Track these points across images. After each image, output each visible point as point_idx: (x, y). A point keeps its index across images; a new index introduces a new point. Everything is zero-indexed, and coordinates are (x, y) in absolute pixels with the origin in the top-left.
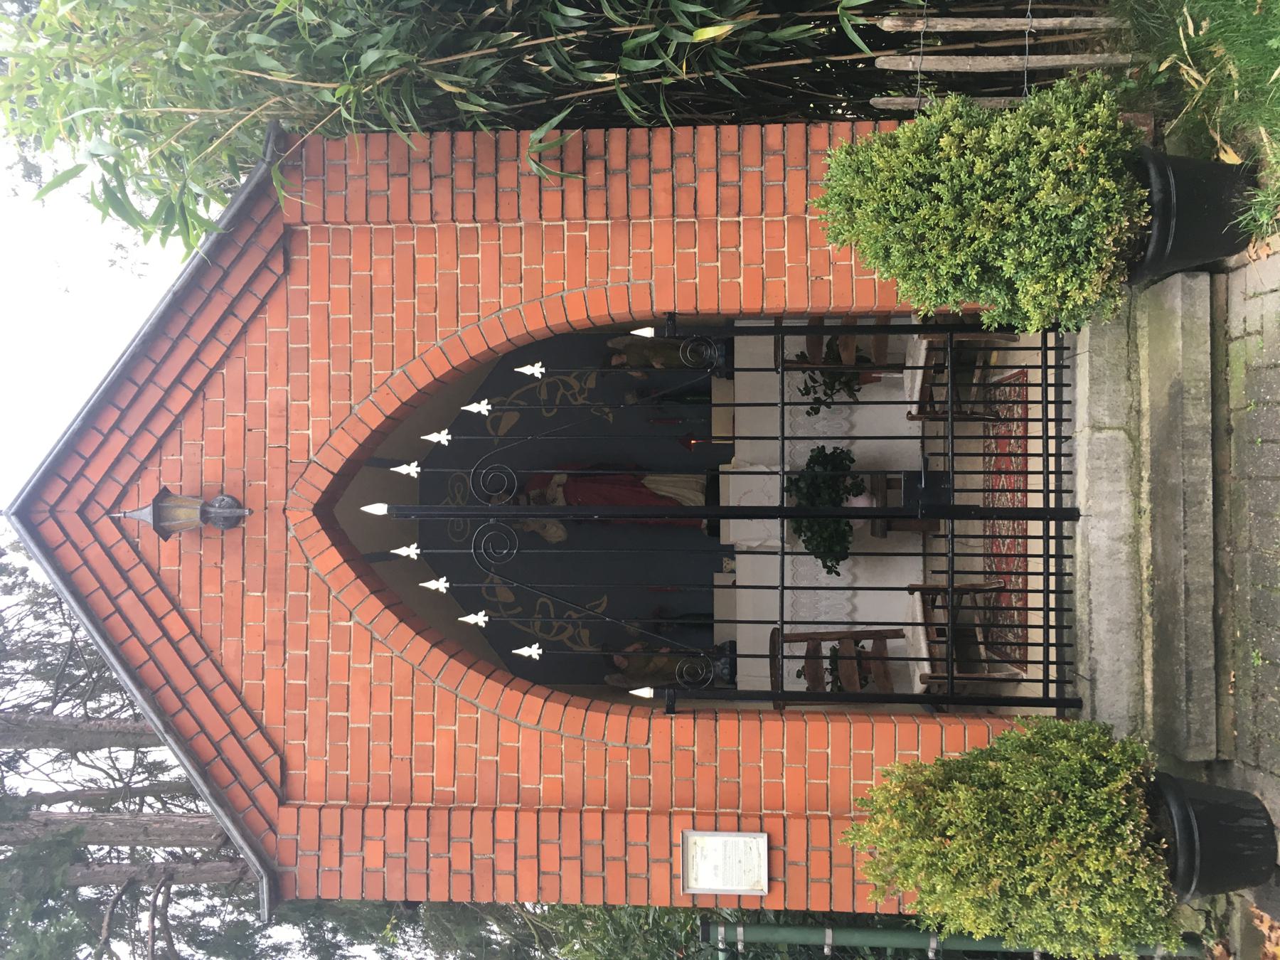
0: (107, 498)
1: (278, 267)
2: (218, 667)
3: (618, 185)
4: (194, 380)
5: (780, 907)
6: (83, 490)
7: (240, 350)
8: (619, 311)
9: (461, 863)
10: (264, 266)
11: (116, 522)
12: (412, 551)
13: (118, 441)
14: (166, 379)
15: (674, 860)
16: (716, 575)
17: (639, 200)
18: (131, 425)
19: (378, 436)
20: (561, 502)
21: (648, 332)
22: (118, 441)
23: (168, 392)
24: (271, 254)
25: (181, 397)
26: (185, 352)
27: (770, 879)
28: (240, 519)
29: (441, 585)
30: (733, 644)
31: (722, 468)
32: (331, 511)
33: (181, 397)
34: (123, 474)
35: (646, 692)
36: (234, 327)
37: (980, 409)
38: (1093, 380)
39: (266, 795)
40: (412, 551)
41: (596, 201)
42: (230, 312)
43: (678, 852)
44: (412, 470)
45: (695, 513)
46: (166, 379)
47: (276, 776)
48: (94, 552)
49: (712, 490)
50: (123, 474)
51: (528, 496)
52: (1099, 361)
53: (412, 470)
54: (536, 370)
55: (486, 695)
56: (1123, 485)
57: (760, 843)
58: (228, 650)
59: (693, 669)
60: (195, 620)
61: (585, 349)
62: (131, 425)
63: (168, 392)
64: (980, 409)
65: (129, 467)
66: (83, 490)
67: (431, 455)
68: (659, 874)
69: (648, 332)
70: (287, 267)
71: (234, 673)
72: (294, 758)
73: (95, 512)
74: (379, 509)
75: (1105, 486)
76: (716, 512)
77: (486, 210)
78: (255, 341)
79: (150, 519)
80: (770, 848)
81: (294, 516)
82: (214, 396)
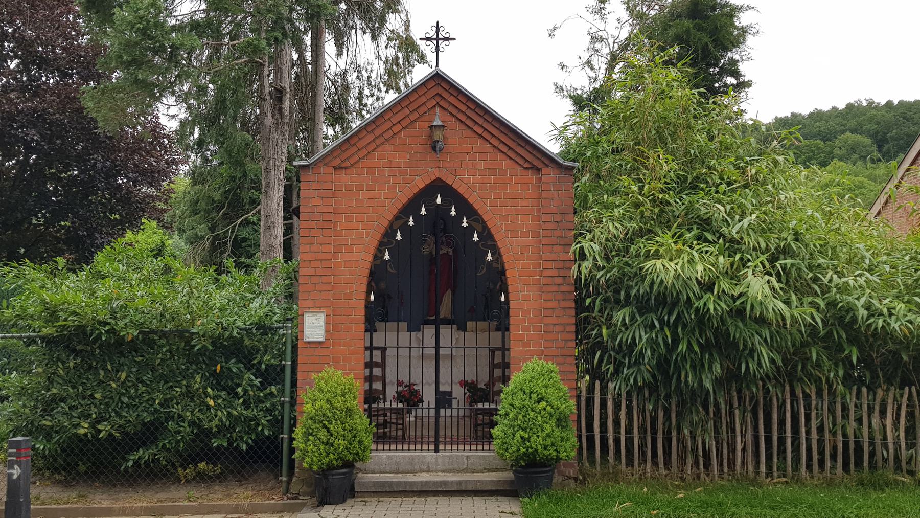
0: (442, 103)
1: (526, 165)
2: (382, 143)
3: (555, 288)
4: (485, 134)
5: (299, 346)
6: (446, 95)
7: (497, 151)
9: (313, 233)
10: (527, 161)
11: (434, 106)
12: (423, 212)
13: (463, 108)
14: (485, 125)
15: (317, 308)
16: (405, 324)
17: (549, 296)
18: (469, 112)
19: (465, 201)
20: (441, 252)
21: (503, 299)
22: (463, 108)
23: (481, 126)
24: (532, 164)
25: (480, 131)
26: (495, 132)
27: (309, 342)
28: (435, 151)
29: (411, 223)
30: (376, 331)
31: (455, 326)
32: (438, 186)
33: (480, 131)
34: (450, 109)
35: (372, 298)
36: (505, 149)
37: (480, 434)
38: (484, 456)
39: (337, 162)
40: (423, 212)
41: (549, 280)
42: (510, 148)
43: (318, 310)
44: (453, 213)
45: (437, 313)
46: (485, 125)
47: (343, 165)
48: (424, 99)
49: (447, 322)
50: (450, 109)
52: (491, 459)
53: (453, 213)
54: (489, 258)
55: (371, 240)
56: (447, 467)
57: (321, 339)
58: (388, 147)
59: (377, 314)
60: (399, 135)
61: (498, 275)
62: (469, 112)
63: (481, 126)
64: (480, 434)
65: (455, 112)
66: (446, 95)
67: (459, 218)
68: (309, 303)
69: (503, 299)
70: (526, 168)
71: (379, 149)
72: (349, 171)
73: (438, 99)
74: (439, 200)
75: (447, 460)
76: (438, 323)
77: (545, 241)
78: (499, 156)
79: (435, 124)
80: (320, 342)
81: (436, 171)
82: (479, 141)
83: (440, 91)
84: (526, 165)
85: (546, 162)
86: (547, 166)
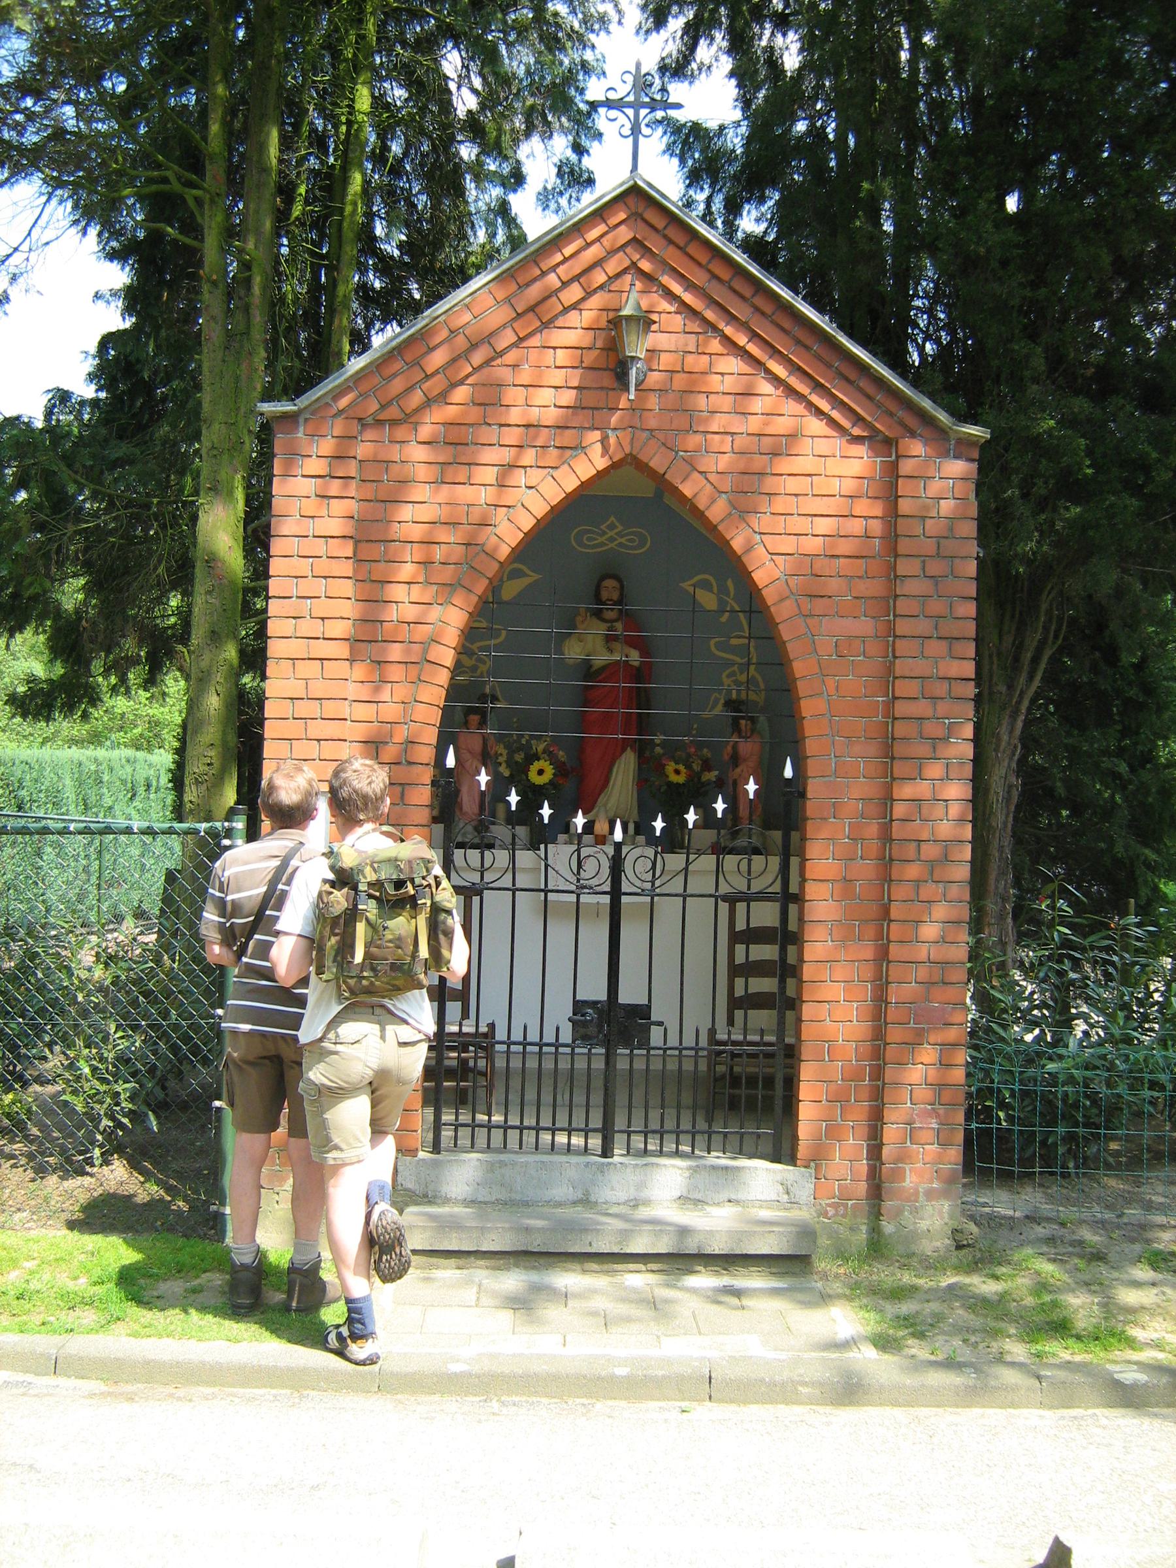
1: (856, 431)
6: (655, 244)
8: (811, 746)
11: (625, 271)
21: (788, 772)
51: (616, 621)
69: (788, 772)
83: (642, 232)
84: (856, 431)
85: (911, 421)
86: (913, 434)
